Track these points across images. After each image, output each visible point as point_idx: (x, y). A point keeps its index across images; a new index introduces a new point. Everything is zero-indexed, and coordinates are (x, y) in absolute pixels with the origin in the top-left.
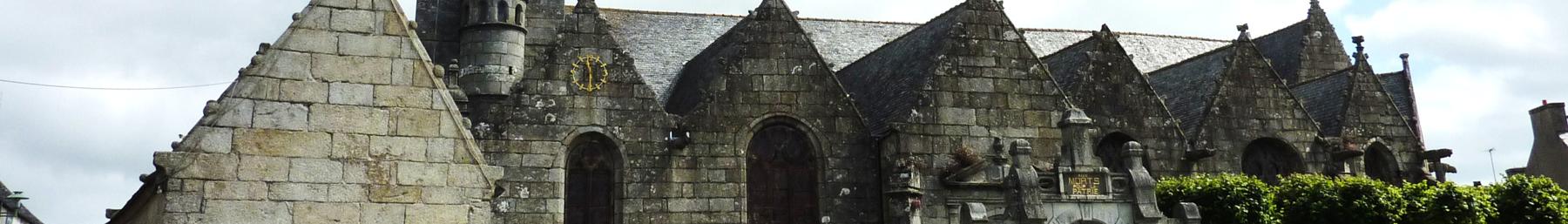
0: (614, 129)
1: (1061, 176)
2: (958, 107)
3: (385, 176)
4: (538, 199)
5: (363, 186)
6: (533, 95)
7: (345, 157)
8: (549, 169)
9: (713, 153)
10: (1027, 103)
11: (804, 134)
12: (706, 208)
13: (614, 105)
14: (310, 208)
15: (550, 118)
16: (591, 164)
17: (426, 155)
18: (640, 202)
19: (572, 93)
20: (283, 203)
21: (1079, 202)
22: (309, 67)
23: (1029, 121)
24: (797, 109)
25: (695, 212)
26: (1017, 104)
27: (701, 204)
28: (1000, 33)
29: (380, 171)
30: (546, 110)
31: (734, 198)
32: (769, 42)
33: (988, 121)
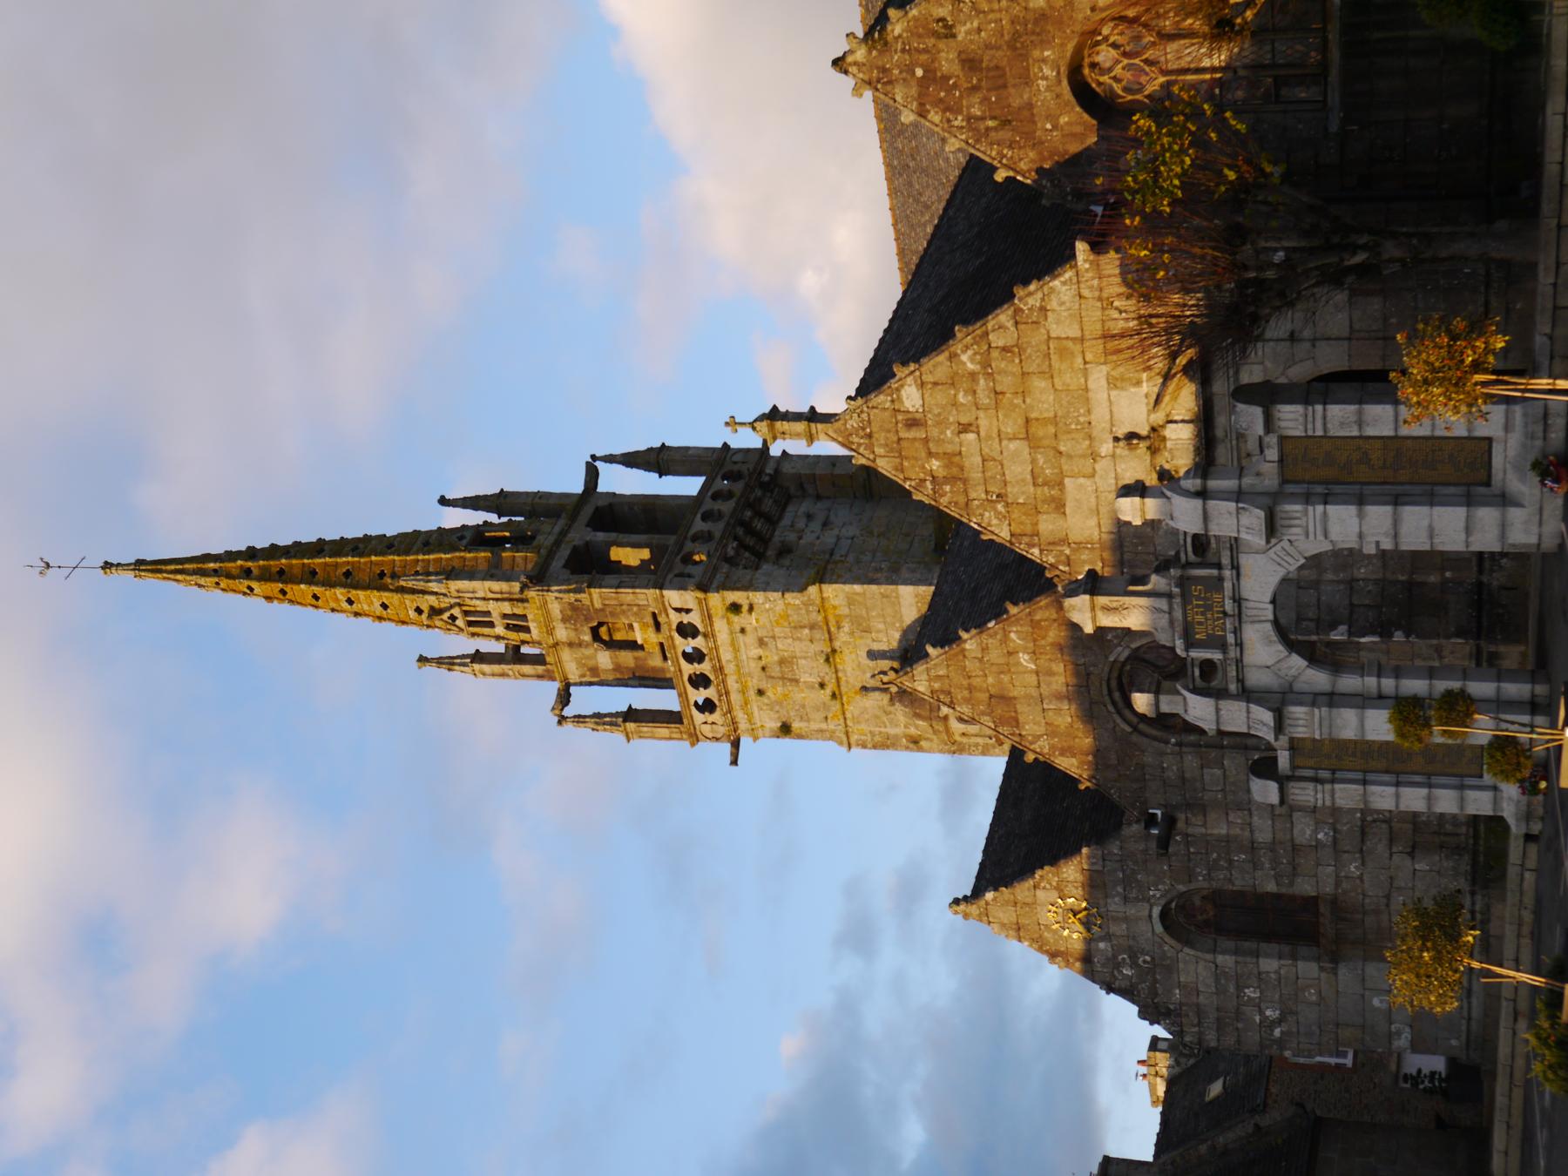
0: (1154, 896)
4: (1260, 979)
6: (1114, 976)
10: (1039, 384)
13: (1118, 892)
15: (1145, 962)
18: (1259, 873)
23: (1075, 381)
24: (1094, 665)
26: (1043, 400)
28: (910, 416)
30: (1134, 964)
32: (987, 695)
33: (1083, 456)
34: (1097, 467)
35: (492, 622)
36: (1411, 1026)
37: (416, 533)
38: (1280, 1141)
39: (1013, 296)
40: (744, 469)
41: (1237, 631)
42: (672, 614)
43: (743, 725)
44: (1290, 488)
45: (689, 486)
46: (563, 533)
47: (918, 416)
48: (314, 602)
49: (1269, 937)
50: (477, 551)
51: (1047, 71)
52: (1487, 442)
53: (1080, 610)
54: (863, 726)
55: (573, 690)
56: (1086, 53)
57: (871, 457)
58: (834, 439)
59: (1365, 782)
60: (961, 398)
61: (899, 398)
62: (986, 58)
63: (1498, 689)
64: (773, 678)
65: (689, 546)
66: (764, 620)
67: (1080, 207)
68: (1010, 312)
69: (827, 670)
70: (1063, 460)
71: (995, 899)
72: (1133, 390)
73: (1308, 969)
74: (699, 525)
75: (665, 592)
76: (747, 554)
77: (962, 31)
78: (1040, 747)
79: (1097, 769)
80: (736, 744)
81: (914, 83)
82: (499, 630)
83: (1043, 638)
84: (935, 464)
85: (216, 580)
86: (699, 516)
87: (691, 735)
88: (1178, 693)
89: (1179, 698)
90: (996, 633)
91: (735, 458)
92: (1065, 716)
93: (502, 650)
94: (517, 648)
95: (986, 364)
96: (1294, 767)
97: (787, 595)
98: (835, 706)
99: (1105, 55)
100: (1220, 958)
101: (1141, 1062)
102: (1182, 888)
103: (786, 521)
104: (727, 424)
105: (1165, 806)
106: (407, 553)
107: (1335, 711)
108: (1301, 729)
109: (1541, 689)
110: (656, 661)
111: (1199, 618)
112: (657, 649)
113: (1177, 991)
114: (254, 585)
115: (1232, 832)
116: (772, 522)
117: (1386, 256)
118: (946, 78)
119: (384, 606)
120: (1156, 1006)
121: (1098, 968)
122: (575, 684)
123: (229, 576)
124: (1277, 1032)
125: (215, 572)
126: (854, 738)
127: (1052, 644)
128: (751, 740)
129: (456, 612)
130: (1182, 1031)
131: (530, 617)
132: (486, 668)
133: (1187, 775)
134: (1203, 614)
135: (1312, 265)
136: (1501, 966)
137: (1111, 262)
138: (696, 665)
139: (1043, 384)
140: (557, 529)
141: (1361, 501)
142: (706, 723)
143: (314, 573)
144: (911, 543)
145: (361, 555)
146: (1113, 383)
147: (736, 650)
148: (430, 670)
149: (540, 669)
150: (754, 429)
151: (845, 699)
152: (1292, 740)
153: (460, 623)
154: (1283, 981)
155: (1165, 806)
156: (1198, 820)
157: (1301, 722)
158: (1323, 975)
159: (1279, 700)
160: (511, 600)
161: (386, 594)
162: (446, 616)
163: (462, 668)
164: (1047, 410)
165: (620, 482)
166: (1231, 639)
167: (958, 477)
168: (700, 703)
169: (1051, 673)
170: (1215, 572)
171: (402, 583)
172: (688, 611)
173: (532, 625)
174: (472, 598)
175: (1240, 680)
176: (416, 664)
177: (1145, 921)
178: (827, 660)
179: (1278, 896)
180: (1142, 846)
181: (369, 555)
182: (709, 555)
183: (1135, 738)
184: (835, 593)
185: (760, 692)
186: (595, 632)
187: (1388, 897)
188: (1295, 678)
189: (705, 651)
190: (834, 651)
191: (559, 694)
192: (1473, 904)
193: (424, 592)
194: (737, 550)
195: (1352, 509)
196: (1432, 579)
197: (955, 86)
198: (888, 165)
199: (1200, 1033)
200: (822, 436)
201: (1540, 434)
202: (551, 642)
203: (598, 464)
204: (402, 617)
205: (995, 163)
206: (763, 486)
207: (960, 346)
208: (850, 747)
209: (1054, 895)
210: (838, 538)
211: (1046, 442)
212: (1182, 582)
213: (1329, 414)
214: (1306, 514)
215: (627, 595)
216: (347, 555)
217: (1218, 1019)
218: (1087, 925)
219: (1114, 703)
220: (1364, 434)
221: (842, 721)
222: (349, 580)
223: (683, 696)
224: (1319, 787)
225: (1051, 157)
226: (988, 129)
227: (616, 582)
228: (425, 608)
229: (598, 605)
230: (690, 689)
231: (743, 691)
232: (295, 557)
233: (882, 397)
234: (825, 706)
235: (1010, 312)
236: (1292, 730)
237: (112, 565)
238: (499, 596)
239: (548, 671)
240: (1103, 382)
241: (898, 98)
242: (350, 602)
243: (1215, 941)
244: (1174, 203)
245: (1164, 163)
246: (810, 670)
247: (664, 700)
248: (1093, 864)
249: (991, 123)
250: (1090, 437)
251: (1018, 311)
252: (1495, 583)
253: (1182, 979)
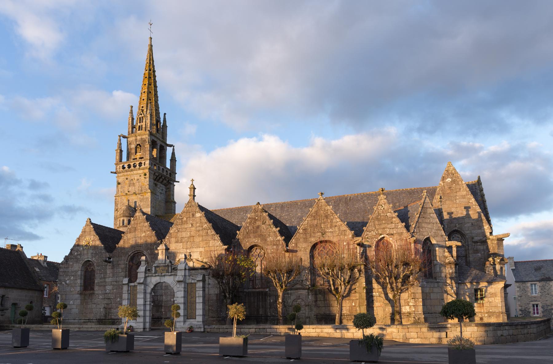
2: (177, 243)
4: (75, 279)
10: (201, 239)
13: (93, 252)
15: (78, 257)
18: (99, 279)
23: (201, 245)
25: (113, 282)
26: (198, 239)
30: (77, 255)
34: (185, 249)
35: (140, 123)
37: (159, 108)
38: (38, 284)
39: (217, 234)
40: (172, 177)
41: (158, 276)
42: (144, 161)
43: (119, 175)
44: (186, 285)
45: (168, 166)
46: (159, 139)
47: (195, 216)
48: (144, 84)
49: (85, 282)
50: (155, 121)
51: (256, 241)
52: (195, 318)
53: (162, 247)
54: (120, 200)
55: (126, 139)
56: (259, 247)
57: (186, 207)
58: (190, 200)
59: (128, 299)
60: (198, 224)
61: (198, 213)
62: (259, 230)
63: (147, 322)
64: (130, 181)
65: (157, 166)
66: (143, 180)
67: (232, 246)
68: (214, 234)
69: (132, 193)
70: (186, 243)
71: (91, 227)
72: (199, 256)
73: (78, 289)
74: (161, 168)
75: (149, 160)
76: (155, 177)
77: (264, 226)
78: (125, 237)
79: (120, 248)
80: (115, 173)
81: (255, 217)
82: (139, 124)
83: (148, 238)
84: (185, 219)
85: (149, 63)
86: (163, 168)
87: (117, 164)
88: (145, 265)
89: (144, 265)
90: (149, 229)
91: (174, 175)
92: (132, 242)
93: (134, 124)
94: (135, 128)
95: (204, 229)
96: (130, 286)
97: (148, 185)
98: (124, 194)
99: (258, 251)
100: (80, 272)
101: (41, 254)
102: (95, 264)
103: (161, 185)
104: (193, 179)
105: (113, 261)
106: (155, 106)
107: (143, 293)
108: (139, 287)
109: (148, 330)
110: (133, 157)
111: (161, 269)
112: (135, 158)
113: (72, 263)
114: (148, 71)
116: (161, 183)
117: (227, 300)
118: (255, 223)
119: (143, 100)
120: (68, 259)
121: (76, 248)
122: (127, 140)
123: (149, 66)
124: (63, 283)
125: (150, 63)
126: (117, 197)
127: (147, 240)
128: (116, 176)
129: (143, 115)
130: (63, 264)
131: (142, 131)
132: (130, 121)
133: (120, 265)
134: (162, 269)
135: (227, 288)
136: (442, 322)
137: (224, 252)
138: (133, 166)
139: (201, 239)
140: (160, 138)
141: (184, 297)
142: (120, 167)
143: (150, 85)
144: (157, 210)
145: (154, 96)
146: (201, 252)
147: (136, 174)
148: (130, 108)
149: (131, 132)
150: (192, 185)
151: (126, 196)
152: (137, 286)
153: (140, 116)
154: (75, 284)
155: (113, 261)
156: (110, 267)
157: (140, 287)
158: (77, 292)
159: (145, 283)
160: (146, 127)
161: (146, 101)
162: (142, 113)
163: (130, 115)
164: (196, 240)
165: (169, 150)
166: (157, 274)
167: (182, 223)
168: (124, 166)
169: (141, 239)
170: (170, 271)
171: (149, 104)
172: (145, 165)
173: (140, 131)
174: (146, 119)
175: (148, 276)
176: (131, 105)
177: (87, 257)
178: (134, 193)
179: (94, 283)
180: (104, 256)
181: (154, 97)
182: (156, 170)
183: (127, 255)
184: (149, 195)
185: (127, 179)
186: (139, 145)
187: (95, 304)
188: (149, 286)
189: (136, 168)
190: (136, 194)
191: (125, 136)
192: (94, 320)
193: (147, 109)
194: (157, 175)
195: (183, 296)
196: (163, 310)
197: (254, 224)
198: (232, 209)
199: (62, 268)
200: (190, 198)
201: (197, 327)
202: (137, 135)
203: (173, 147)
204: (141, 103)
205: (240, 231)
206: (169, 181)
207: (208, 224)
208: (115, 197)
209: (93, 239)
210: (158, 196)
211: (189, 240)
212: (168, 266)
213: (201, 291)
214: (182, 288)
215: (148, 152)
216: (154, 92)
217: (66, 271)
218: (86, 246)
219: (135, 251)
220: (197, 298)
221: (121, 195)
222: (149, 93)
223: (126, 163)
224: (127, 291)
225: (242, 241)
226: (246, 230)
227: (150, 150)
228: (143, 109)
229: (146, 146)
230: (128, 164)
231: (127, 175)
232: (154, 81)
233: (198, 209)
234: (124, 192)
235: (214, 234)
236: (139, 286)
237: (151, 39)
238: (147, 125)
239: (130, 134)
240: (201, 251)
241: (252, 214)
242: (144, 92)
243: (83, 271)
244: (239, 264)
245: (245, 262)
246: (132, 189)
247: (124, 159)
248: (100, 247)
249: (247, 230)
250: (190, 248)
251: (215, 235)
252: (162, 321)
253: (74, 264)
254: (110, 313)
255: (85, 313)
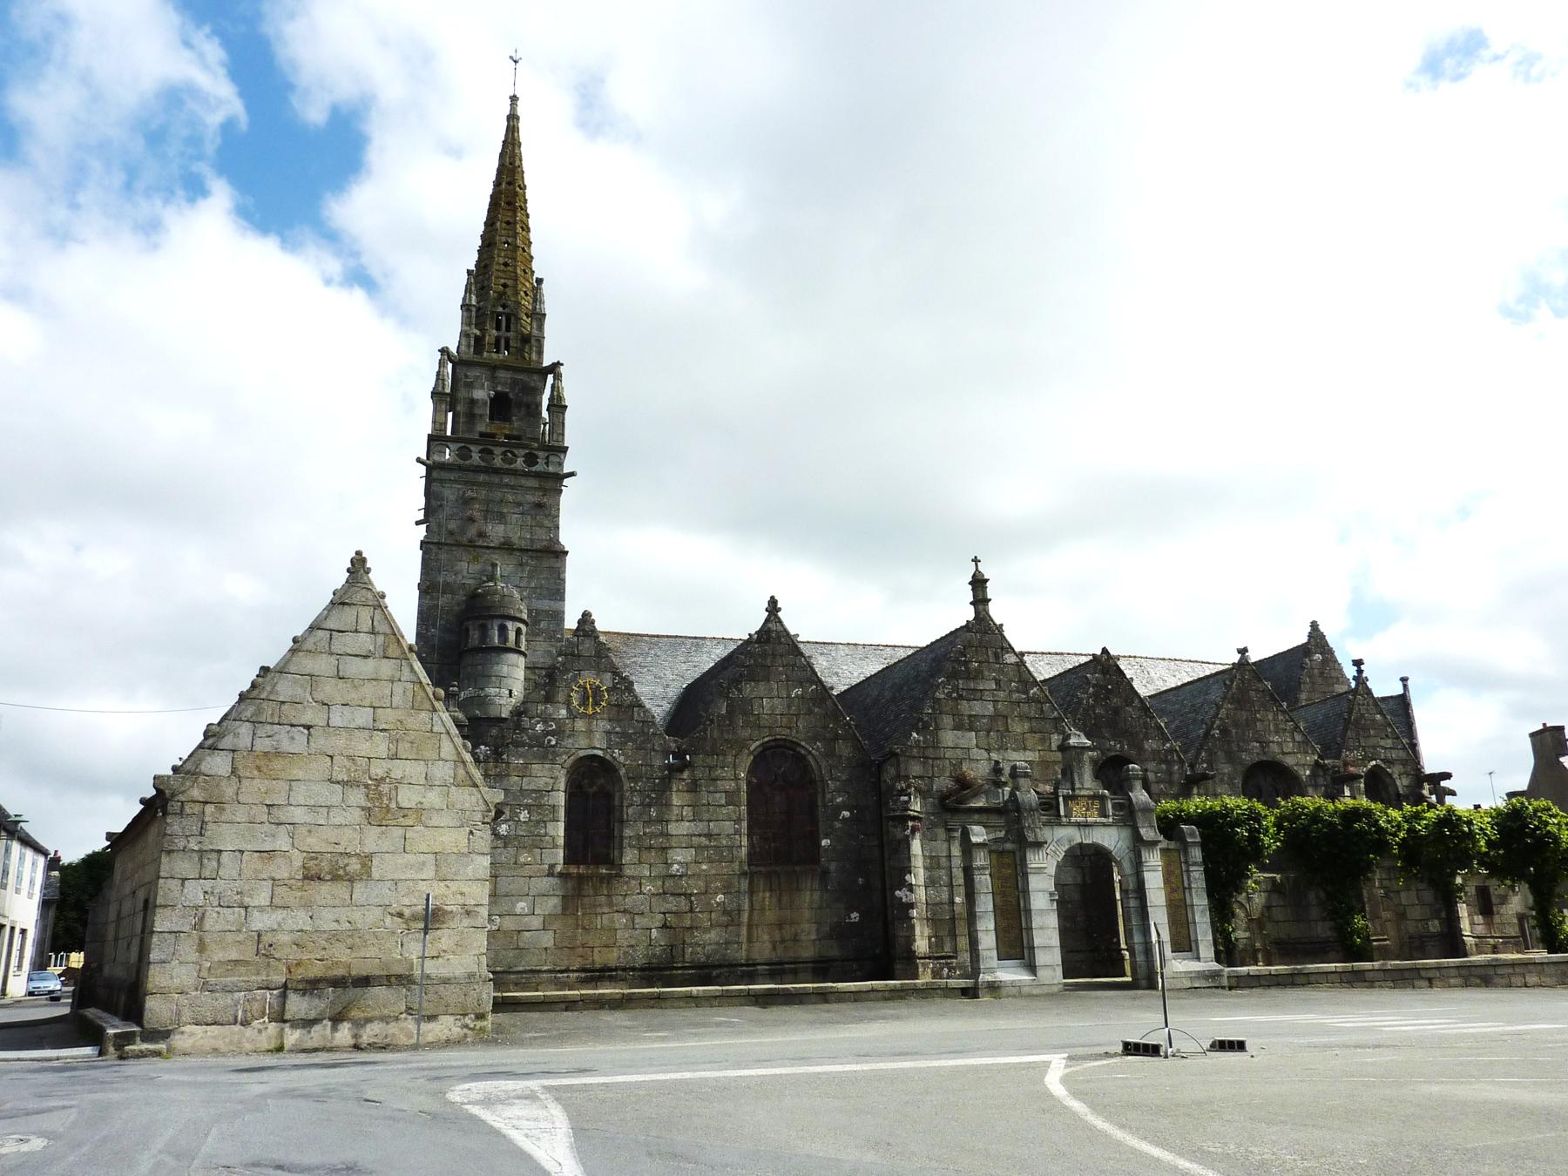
0: (614, 752)
1: (1061, 799)
3: (385, 799)
4: (538, 822)
5: (363, 809)
6: (533, 718)
7: (345, 780)
8: (549, 791)
9: (713, 776)
10: (1027, 726)
11: (804, 757)
12: (706, 831)
13: (614, 728)
14: (310, 831)
15: (550, 741)
16: (591, 787)
17: (426, 778)
18: (640, 825)
19: (573, 716)
20: (283, 826)
21: (1078, 825)
22: (309, 689)
23: (1029, 744)
24: (797, 732)
25: (695, 835)
26: (1018, 727)
27: (701, 827)
29: (380, 794)
30: (546, 733)
31: (734, 821)
32: (769, 665)
33: (989, 744)
36: (499, 930)
102: (622, 771)
115: (675, 808)
187: (625, 911)
254: (691, 945)
255: (583, 946)
